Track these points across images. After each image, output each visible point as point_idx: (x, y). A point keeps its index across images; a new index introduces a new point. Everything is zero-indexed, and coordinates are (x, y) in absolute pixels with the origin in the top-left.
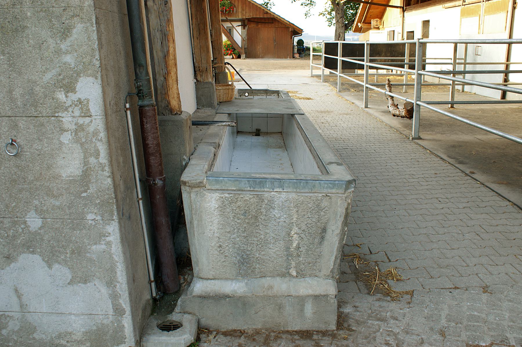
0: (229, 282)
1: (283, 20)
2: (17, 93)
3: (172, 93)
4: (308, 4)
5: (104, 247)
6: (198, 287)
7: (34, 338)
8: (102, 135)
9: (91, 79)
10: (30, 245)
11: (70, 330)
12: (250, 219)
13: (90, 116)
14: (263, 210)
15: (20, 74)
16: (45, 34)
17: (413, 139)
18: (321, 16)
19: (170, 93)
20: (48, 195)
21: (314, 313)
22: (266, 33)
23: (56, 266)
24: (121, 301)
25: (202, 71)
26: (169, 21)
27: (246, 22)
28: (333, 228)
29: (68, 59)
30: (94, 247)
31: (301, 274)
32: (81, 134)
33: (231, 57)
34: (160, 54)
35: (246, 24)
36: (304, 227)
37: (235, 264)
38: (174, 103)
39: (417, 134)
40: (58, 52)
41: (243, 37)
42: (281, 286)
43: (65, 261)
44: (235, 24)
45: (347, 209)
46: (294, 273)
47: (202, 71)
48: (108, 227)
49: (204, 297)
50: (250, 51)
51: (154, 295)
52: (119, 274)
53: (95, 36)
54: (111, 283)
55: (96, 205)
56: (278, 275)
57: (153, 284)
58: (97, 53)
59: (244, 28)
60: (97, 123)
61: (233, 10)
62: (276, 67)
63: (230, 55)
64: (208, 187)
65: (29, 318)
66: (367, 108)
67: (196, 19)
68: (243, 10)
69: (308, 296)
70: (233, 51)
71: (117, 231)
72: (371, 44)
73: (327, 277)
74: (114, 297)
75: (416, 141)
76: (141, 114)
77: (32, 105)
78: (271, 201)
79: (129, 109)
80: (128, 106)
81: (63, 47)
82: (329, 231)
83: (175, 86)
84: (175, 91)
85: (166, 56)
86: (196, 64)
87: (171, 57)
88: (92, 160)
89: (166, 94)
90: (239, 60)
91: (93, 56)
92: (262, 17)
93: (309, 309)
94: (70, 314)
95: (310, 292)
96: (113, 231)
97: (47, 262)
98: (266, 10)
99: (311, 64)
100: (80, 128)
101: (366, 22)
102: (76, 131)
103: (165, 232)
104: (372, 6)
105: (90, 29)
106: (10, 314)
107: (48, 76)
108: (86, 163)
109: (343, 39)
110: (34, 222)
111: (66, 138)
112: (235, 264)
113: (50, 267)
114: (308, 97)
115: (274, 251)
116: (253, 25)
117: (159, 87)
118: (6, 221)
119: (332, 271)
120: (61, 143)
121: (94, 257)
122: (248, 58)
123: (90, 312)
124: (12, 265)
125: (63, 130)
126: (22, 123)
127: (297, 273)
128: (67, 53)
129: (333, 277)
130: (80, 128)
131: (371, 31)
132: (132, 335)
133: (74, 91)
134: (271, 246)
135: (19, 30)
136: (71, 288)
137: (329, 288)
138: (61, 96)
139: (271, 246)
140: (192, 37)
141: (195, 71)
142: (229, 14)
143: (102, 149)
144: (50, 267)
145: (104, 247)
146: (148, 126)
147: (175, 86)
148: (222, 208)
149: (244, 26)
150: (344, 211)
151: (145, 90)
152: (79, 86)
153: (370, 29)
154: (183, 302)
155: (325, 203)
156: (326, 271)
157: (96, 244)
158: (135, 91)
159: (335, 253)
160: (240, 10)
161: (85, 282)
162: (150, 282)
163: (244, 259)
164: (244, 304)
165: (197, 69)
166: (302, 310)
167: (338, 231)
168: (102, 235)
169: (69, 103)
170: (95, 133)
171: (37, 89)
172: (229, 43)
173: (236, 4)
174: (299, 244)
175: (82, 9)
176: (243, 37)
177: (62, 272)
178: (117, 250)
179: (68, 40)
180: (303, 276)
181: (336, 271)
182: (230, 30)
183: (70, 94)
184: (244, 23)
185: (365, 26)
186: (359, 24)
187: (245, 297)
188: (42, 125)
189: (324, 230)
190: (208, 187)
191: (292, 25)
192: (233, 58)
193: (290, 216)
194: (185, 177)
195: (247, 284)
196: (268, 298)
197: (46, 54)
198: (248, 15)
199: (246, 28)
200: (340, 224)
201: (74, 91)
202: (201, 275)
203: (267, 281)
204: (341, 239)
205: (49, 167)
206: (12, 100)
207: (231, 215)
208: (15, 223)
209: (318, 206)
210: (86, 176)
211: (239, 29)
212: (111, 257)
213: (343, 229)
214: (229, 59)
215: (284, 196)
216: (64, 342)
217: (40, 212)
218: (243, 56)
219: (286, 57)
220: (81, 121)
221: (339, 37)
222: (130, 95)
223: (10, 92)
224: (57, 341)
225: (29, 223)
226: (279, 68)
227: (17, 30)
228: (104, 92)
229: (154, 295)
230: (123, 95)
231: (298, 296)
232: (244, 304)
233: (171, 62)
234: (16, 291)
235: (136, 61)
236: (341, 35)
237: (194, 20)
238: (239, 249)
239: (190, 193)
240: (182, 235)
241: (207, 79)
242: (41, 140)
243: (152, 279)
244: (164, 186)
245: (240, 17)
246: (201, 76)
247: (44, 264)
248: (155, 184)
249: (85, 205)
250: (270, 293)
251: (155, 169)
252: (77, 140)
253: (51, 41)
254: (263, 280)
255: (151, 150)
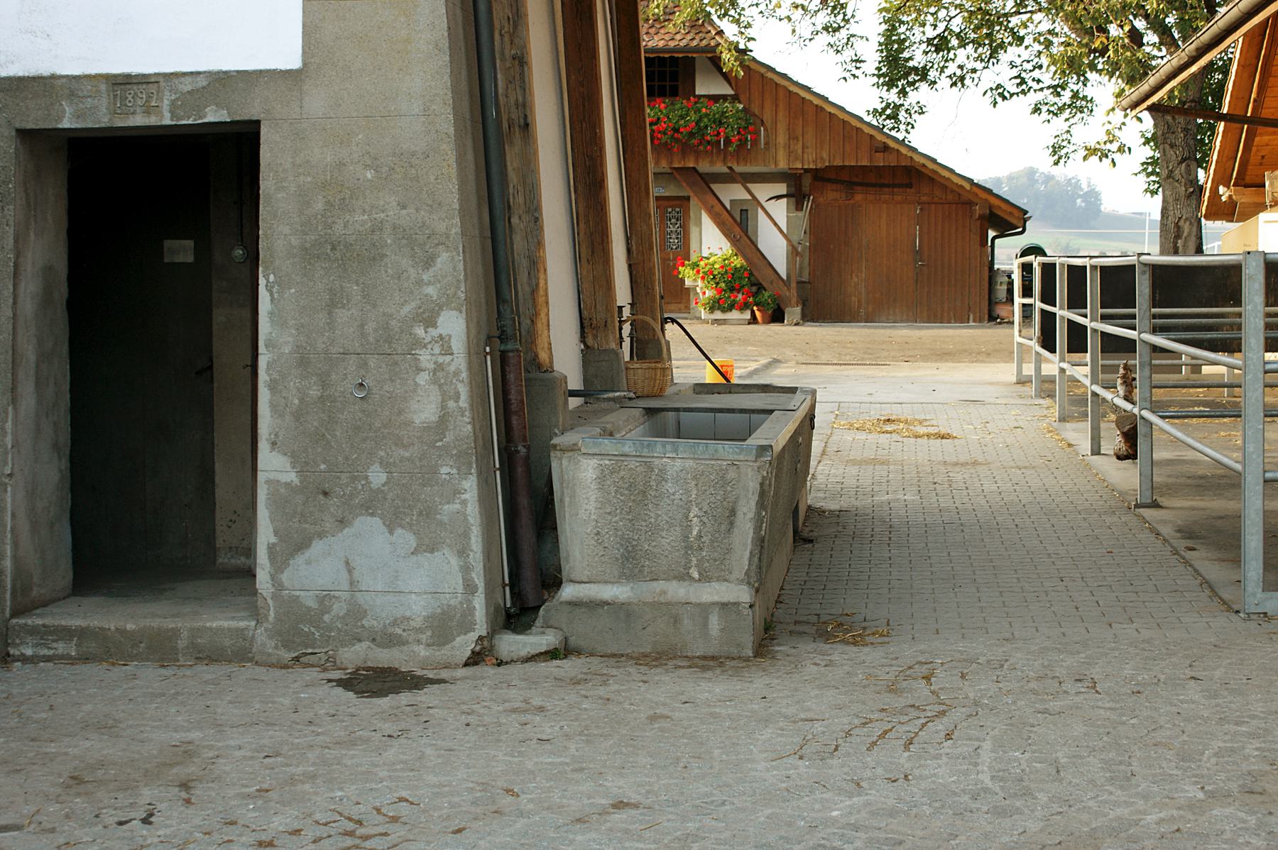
0: (609, 587)
1: (946, 174)
2: (370, 327)
3: (541, 342)
4: (1061, 109)
5: (458, 506)
6: (568, 592)
7: (363, 626)
8: (464, 375)
9: (455, 313)
10: (369, 508)
11: (408, 614)
12: (635, 493)
13: (452, 354)
14: (653, 483)
15: (375, 306)
16: (405, 262)
17: (1137, 506)
18: (1095, 159)
19: (539, 341)
20: (396, 445)
21: (722, 630)
22: (885, 226)
23: (399, 531)
24: (474, 575)
25: (597, 328)
26: (540, 244)
27: (807, 181)
28: (745, 509)
29: (430, 290)
30: (446, 507)
31: (705, 578)
32: (440, 374)
33: (748, 315)
34: (527, 289)
35: (806, 189)
36: (706, 508)
37: (617, 559)
38: (543, 356)
39: (1148, 493)
40: (420, 283)
41: (795, 239)
42: (677, 591)
43: (410, 525)
44: (763, 191)
45: (762, 484)
46: (696, 575)
47: (597, 328)
48: (464, 482)
49: (574, 604)
50: (817, 294)
51: (508, 605)
52: (473, 540)
53: (461, 266)
54: (462, 552)
55: (452, 456)
56: (675, 578)
57: (507, 589)
58: (463, 284)
59: (799, 207)
60: (459, 361)
61: (755, 142)
62: (909, 355)
63: (743, 307)
64: (583, 451)
65: (360, 597)
66: (1099, 454)
67: (587, 222)
68: (792, 137)
69: (713, 604)
70: (755, 295)
71: (475, 487)
72: (1104, 269)
73: (741, 582)
74: (466, 569)
75: (1141, 510)
76: (503, 361)
77: (386, 341)
78: (663, 470)
79: (490, 353)
80: (488, 349)
81: (425, 277)
82: (740, 514)
83: (546, 332)
84: (546, 340)
85: (534, 291)
86: (585, 313)
87: (541, 292)
88: (451, 404)
89: (533, 342)
90: (775, 327)
91: (458, 288)
92: (865, 163)
93: (715, 623)
94: (411, 592)
95: (716, 599)
96: (470, 486)
97: (388, 526)
98: (879, 137)
99: (1018, 339)
100: (440, 367)
101: (1248, 180)
102: (435, 371)
103: (526, 520)
104: (1261, 129)
105: (457, 258)
106: (337, 594)
107: (406, 309)
108: (443, 407)
109: (1192, 245)
110: (377, 477)
111: (423, 379)
112: (617, 559)
113: (391, 533)
114: (943, 431)
115: (669, 540)
116: (831, 195)
117: (523, 333)
118: (344, 476)
119: (747, 574)
120: (416, 384)
121: (445, 519)
122: (813, 320)
123: (433, 590)
124: (345, 531)
125: (420, 370)
126: (372, 362)
127: (700, 574)
128: (429, 283)
129: (749, 583)
130: (440, 367)
131: (1263, 216)
132: (484, 620)
133: (434, 326)
134: (664, 534)
135: (376, 258)
136: (414, 558)
137: (742, 594)
138: (420, 331)
139: (664, 534)
140: (577, 259)
141: (582, 327)
142: (742, 152)
143: (463, 391)
144: (391, 533)
145: (458, 506)
146: (511, 377)
147: (546, 332)
148: (601, 479)
149: (797, 197)
150: (758, 486)
151: (509, 331)
152: (440, 320)
153: (1261, 207)
154: (547, 611)
155: (732, 474)
156: (739, 573)
157: (448, 503)
158: (497, 333)
159: (749, 547)
160: (782, 138)
161: (432, 551)
162: (504, 586)
163: (629, 552)
164: (628, 615)
165: (586, 323)
166: (705, 625)
167: (751, 515)
168: (457, 492)
169: (428, 339)
170: (457, 374)
171: (393, 323)
172: (738, 262)
173: (767, 117)
174: (700, 531)
175: (448, 237)
176: (795, 239)
177: (406, 539)
178: (473, 511)
179: (432, 270)
180: (709, 580)
181: (753, 574)
182: (744, 212)
183: (430, 330)
184: (800, 188)
185: (1245, 197)
186: (1222, 189)
187: (629, 604)
188: (396, 363)
189: (733, 512)
190: (583, 451)
191: (983, 195)
192: (753, 320)
193: (688, 492)
194: (555, 441)
195: (632, 588)
196: (656, 605)
197: (406, 285)
198: (813, 157)
199: (807, 205)
200: (753, 504)
201: (434, 326)
202: (573, 577)
203: (660, 585)
204: (758, 529)
205: (400, 412)
206: (363, 335)
207: (613, 489)
208: (354, 479)
209: (723, 477)
210: (443, 421)
211: (780, 210)
212: (465, 519)
213: (758, 513)
214: (740, 322)
215: (678, 463)
216: (399, 631)
217: (385, 465)
218: (793, 312)
219: (960, 317)
220: (441, 359)
221: (1178, 237)
222: (489, 338)
223: (362, 326)
224: (390, 630)
225: (371, 479)
226: (925, 358)
227: (374, 259)
228: (468, 327)
229: (508, 605)
230: (483, 338)
231: (699, 604)
232: (628, 615)
233: (541, 300)
234: (347, 563)
235: (500, 298)
236: (1186, 228)
237: (582, 225)
238: (622, 538)
239: (560, 459)
240: (549, 546)
241: (607, 343)
242: (393, 381)
243: (507, 581)
244: (527, 457)
245: (783, 165)
246: (595, 337)
247: (385, 529)
248: (518, 452)
249: (440, 456)
250: (662, 599)
251: (516, 433)
252: (435, 381)
253: (412, 270)
254: (655, 584)
255: (514, 407)
